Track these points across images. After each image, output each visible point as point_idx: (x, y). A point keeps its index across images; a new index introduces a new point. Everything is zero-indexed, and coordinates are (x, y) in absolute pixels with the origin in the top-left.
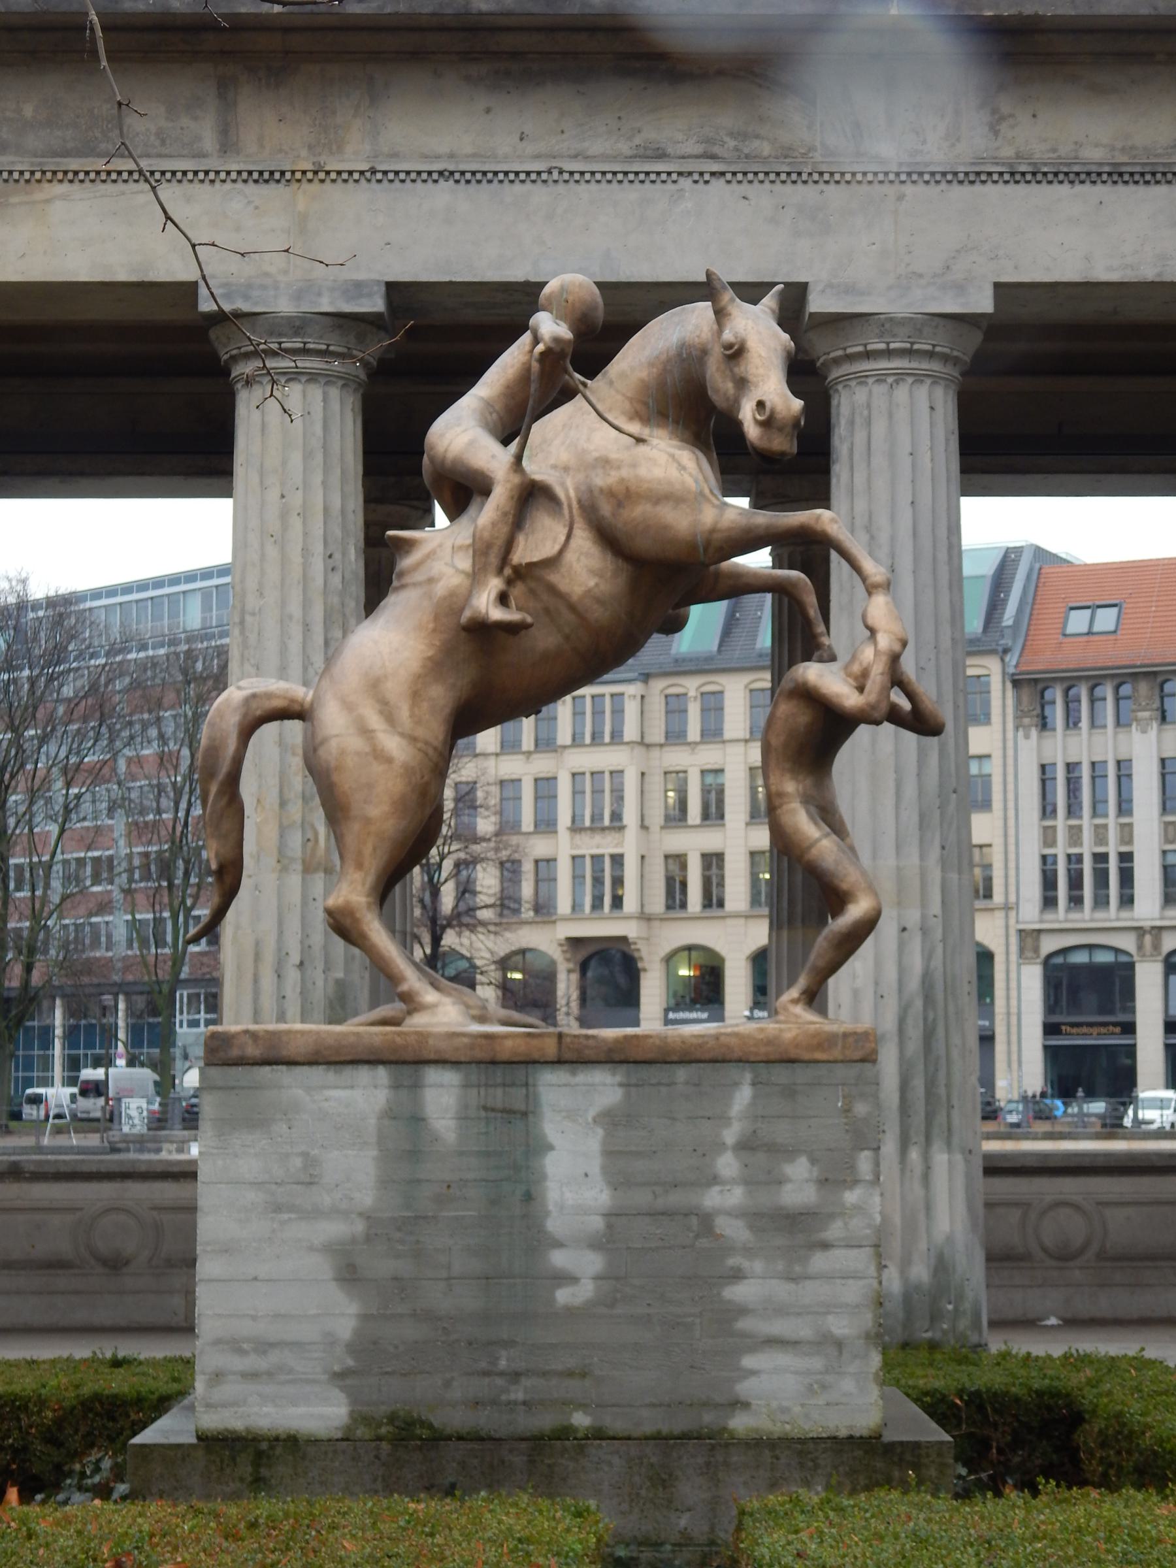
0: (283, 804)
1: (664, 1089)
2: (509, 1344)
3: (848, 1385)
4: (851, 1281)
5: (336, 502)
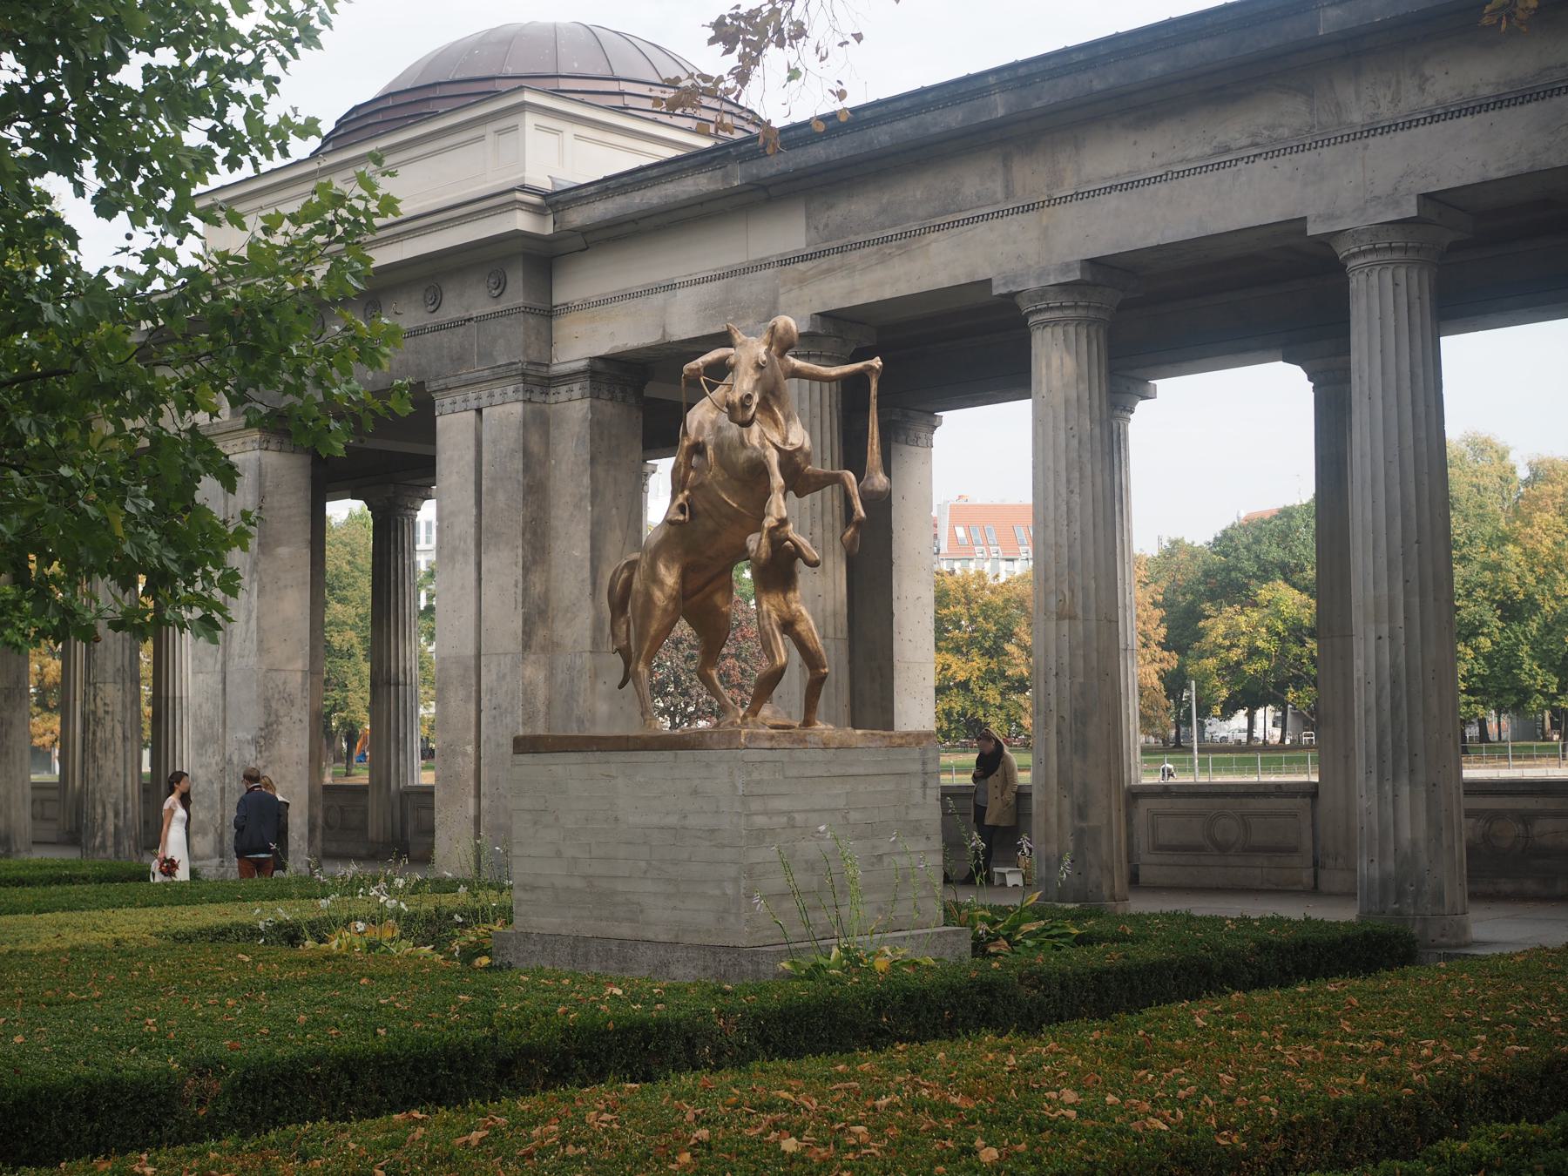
0: (1046, 580)
5: (1096, 403)
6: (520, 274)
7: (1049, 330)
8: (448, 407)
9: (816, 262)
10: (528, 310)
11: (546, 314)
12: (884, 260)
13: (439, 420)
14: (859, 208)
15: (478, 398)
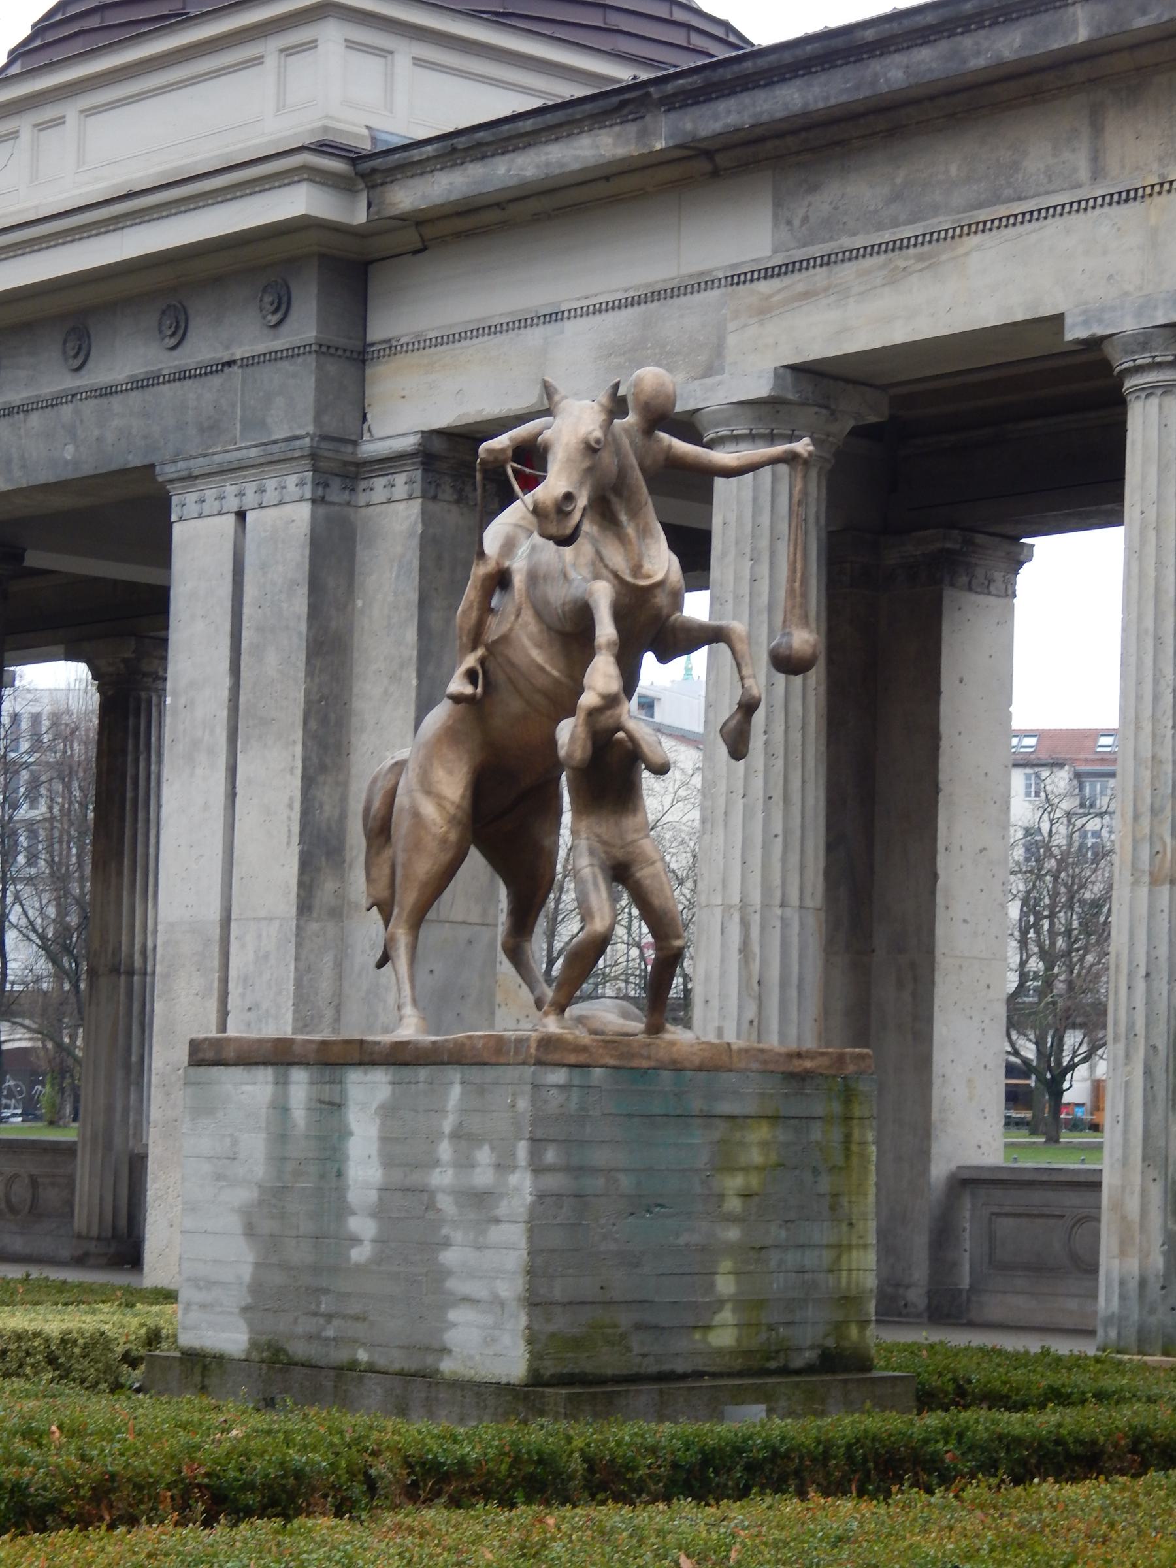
0: (1136, 817)
1: (413, 1086)
2: (326, 1291)
3: (506, 1339)
4: (511, 1252)
6: (314, 289)
7: (1154, 401)
8: (192, 508)
9: (787, 280)
10: (323, 350)
11: (352, 357)
12: (894, 279)
13: (177, 529)
14: (858, 193)
15: (241, 494)
